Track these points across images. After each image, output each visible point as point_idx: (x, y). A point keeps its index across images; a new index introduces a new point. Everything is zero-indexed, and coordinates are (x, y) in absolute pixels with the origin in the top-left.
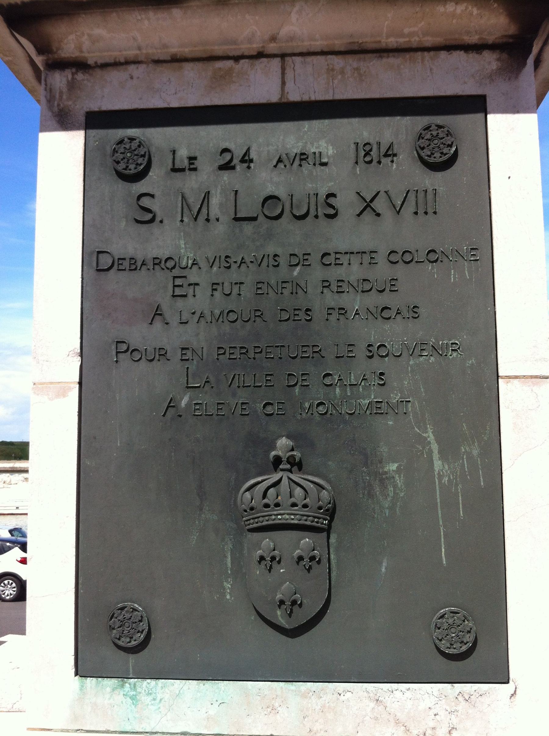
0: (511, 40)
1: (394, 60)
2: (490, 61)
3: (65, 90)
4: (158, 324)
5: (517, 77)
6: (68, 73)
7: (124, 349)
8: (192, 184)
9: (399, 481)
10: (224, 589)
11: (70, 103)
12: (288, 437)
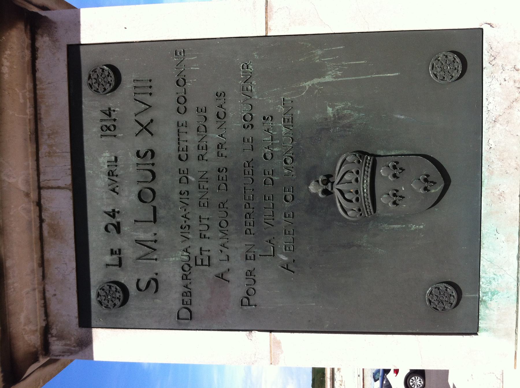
0: (29, 27)
3: (63, 342)
4: (229, 276)
5: (55, 23)
6: (52, 340)
7: (246, 300)
8: (130, 253)
9: (340, 106)
10: (416, 230)
11: (73, 339)
12: (309, 184)
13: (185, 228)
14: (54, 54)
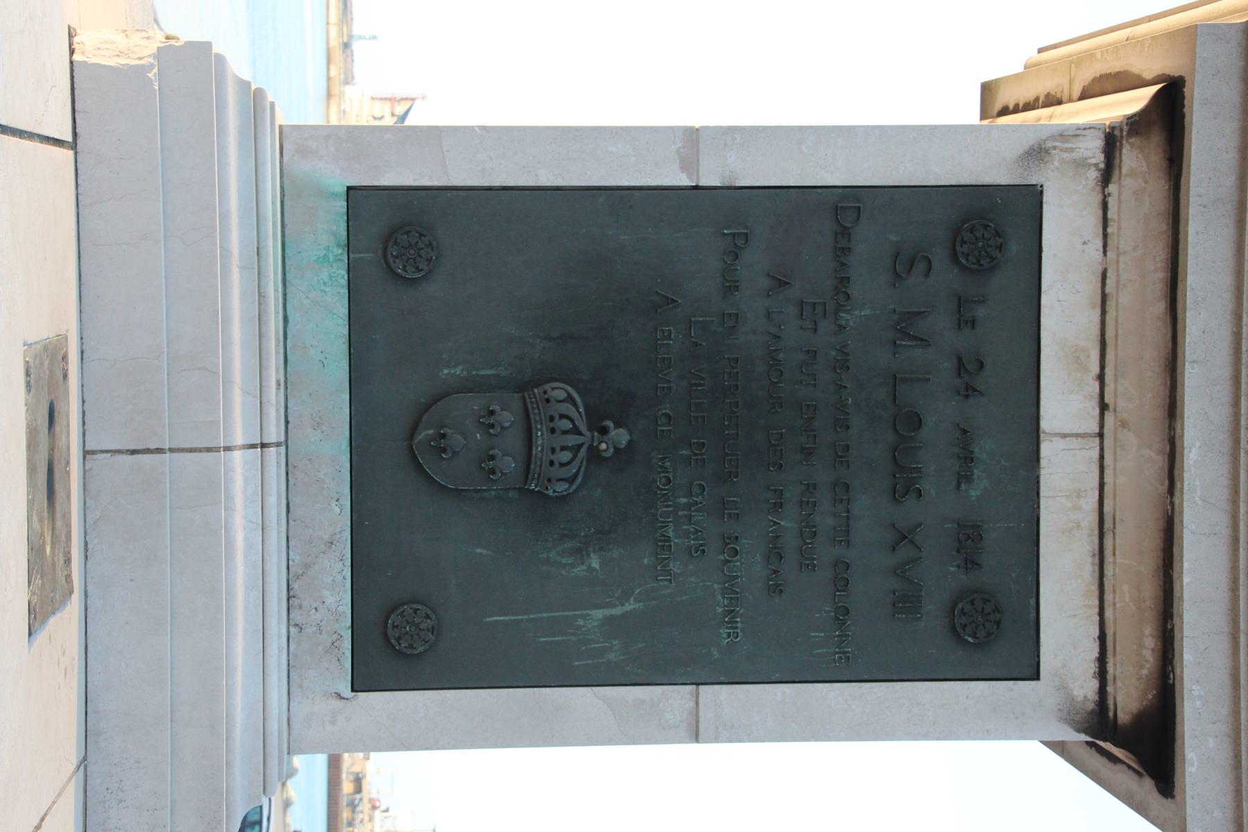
0: (1111, 714)
1: (1089, 570)
2: (1086, 689)
3: (1075, 155)
4: (765, 283)
5: (1061, 719)
6: (1100, 158)
7: (736, 246)
8: (940, 323)
9: (579, 570)
10: (455, 366)
11: (1056, 163)
12: (630, 442)
13: (843, 365)
14: (1064, 666)
